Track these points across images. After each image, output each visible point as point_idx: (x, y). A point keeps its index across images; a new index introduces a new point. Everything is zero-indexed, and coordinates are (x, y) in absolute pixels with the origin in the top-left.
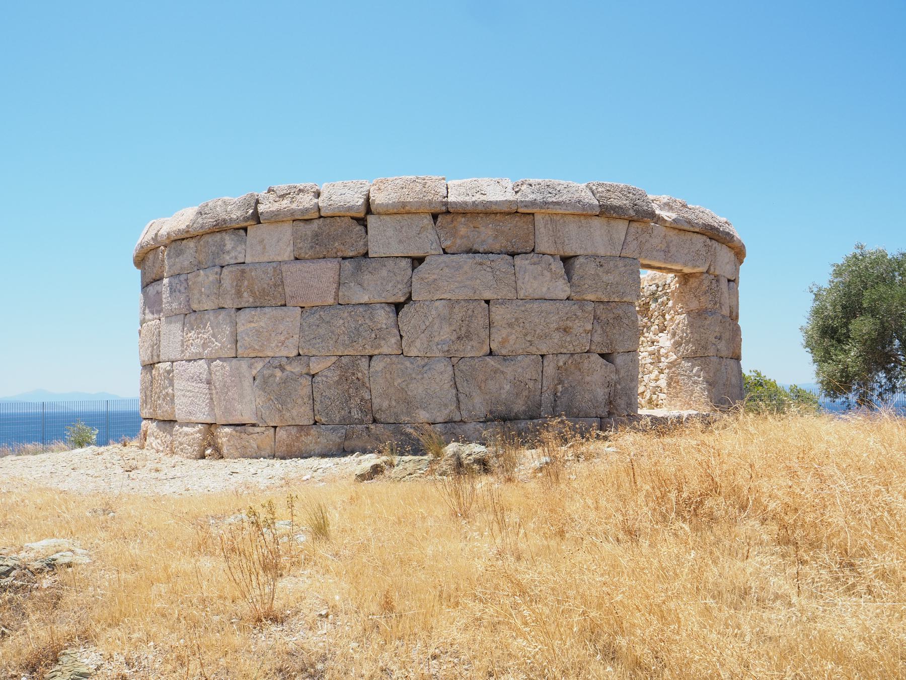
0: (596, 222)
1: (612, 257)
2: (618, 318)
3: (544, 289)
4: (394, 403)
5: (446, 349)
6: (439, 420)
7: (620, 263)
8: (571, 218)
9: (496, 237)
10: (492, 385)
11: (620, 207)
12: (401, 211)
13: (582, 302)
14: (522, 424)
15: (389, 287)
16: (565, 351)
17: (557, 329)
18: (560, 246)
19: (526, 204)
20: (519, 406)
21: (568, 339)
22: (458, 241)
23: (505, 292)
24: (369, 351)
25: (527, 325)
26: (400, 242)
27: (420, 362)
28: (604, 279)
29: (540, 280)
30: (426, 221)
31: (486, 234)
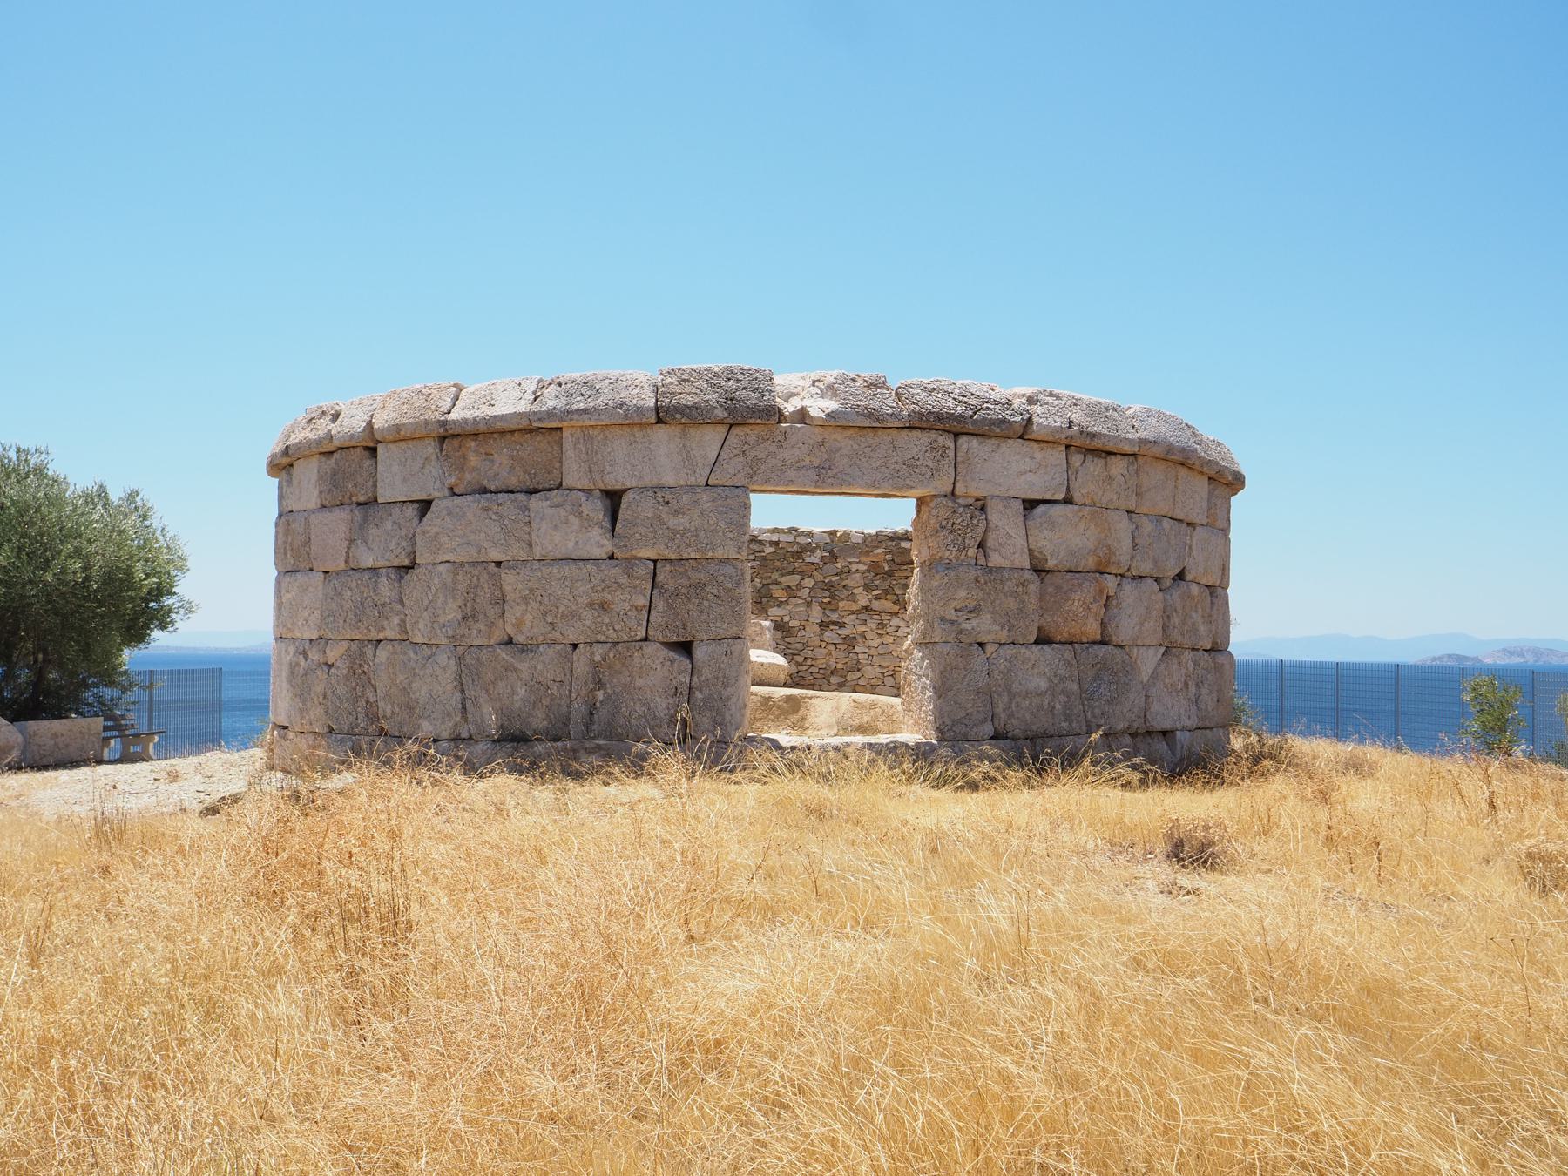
0: (661, 433)
1: (692, 488)
2: (697, 588)
3: (571, 545)
4: (397, 709)
5: (451, 633)
6: (445, 735)
7: (704, 497)
8: (618, 431)
9: (512, 468)
10: (502, 688)
11: (695, 407)
12: (401, 436)
13: (631, 562)
14: (539, 748)
15: (392, 546)
16: (603, 638)
17: (590, 605)
18: (597, 477)
19: (551, 414)
20: (539, 721)
21: (607, 620)
22: (468, 476)
23: (517, 551)
24: (374, 635)
25: (546, 599)
26: (405, 480)
27: (427, 652)
28: (670, 524)
29: (566, 530)
30: (430, 450)
31: (501, 466)
